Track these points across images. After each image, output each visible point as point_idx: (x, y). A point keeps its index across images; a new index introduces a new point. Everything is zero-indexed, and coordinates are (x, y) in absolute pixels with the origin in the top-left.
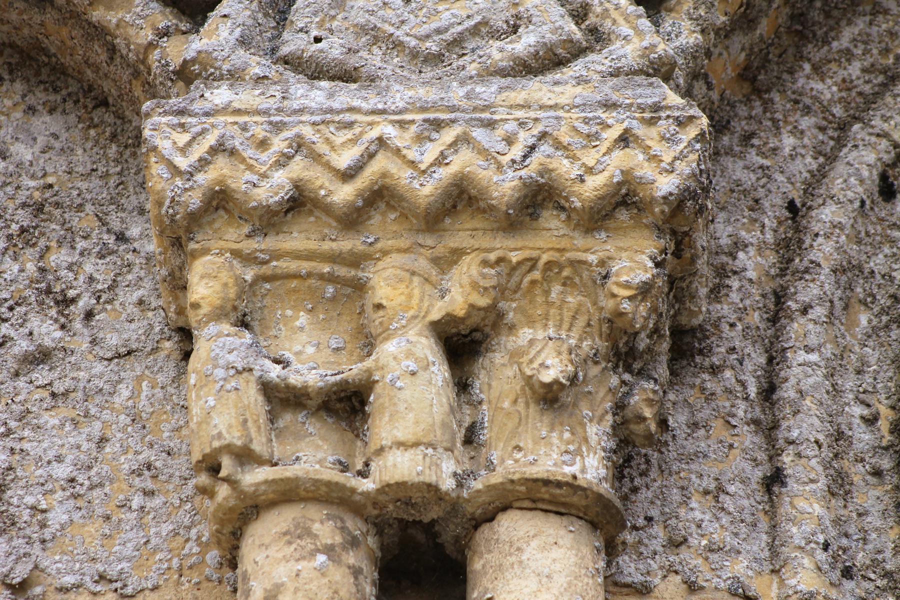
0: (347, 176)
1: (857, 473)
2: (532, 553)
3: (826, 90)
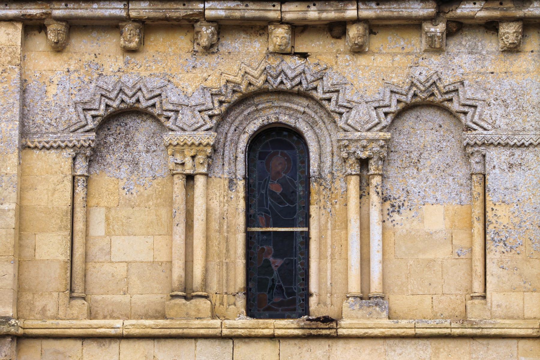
0: (182, 142)
1: (231, 162)
2: (200, 179)
3: (229, 120)
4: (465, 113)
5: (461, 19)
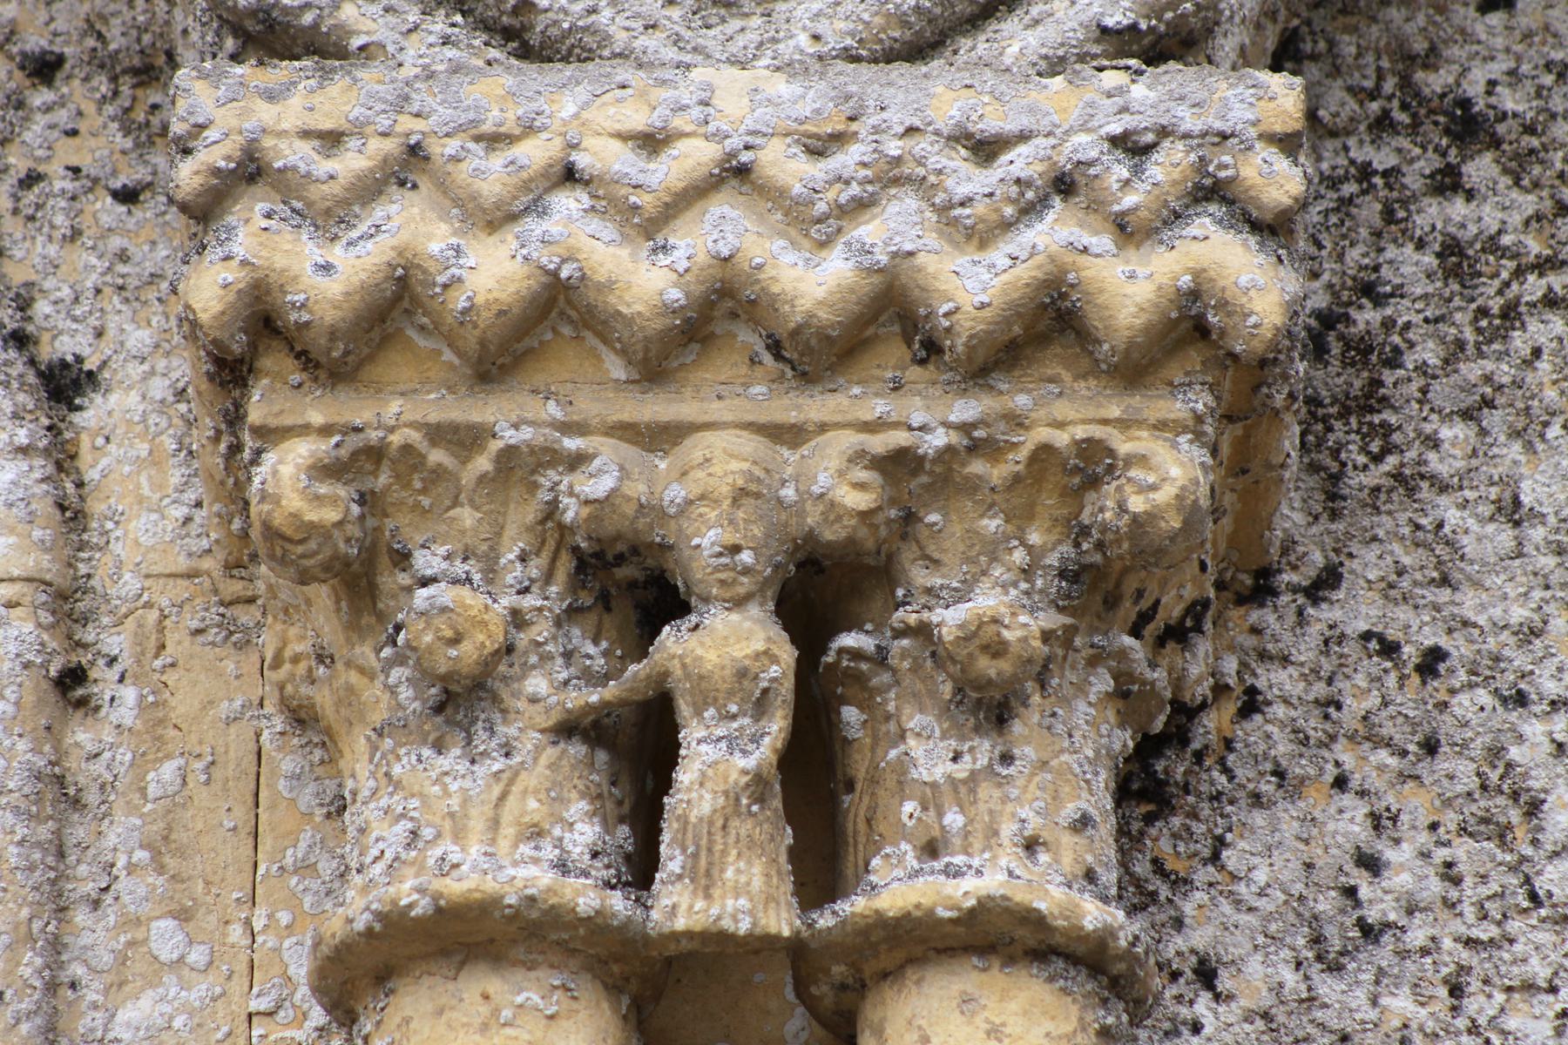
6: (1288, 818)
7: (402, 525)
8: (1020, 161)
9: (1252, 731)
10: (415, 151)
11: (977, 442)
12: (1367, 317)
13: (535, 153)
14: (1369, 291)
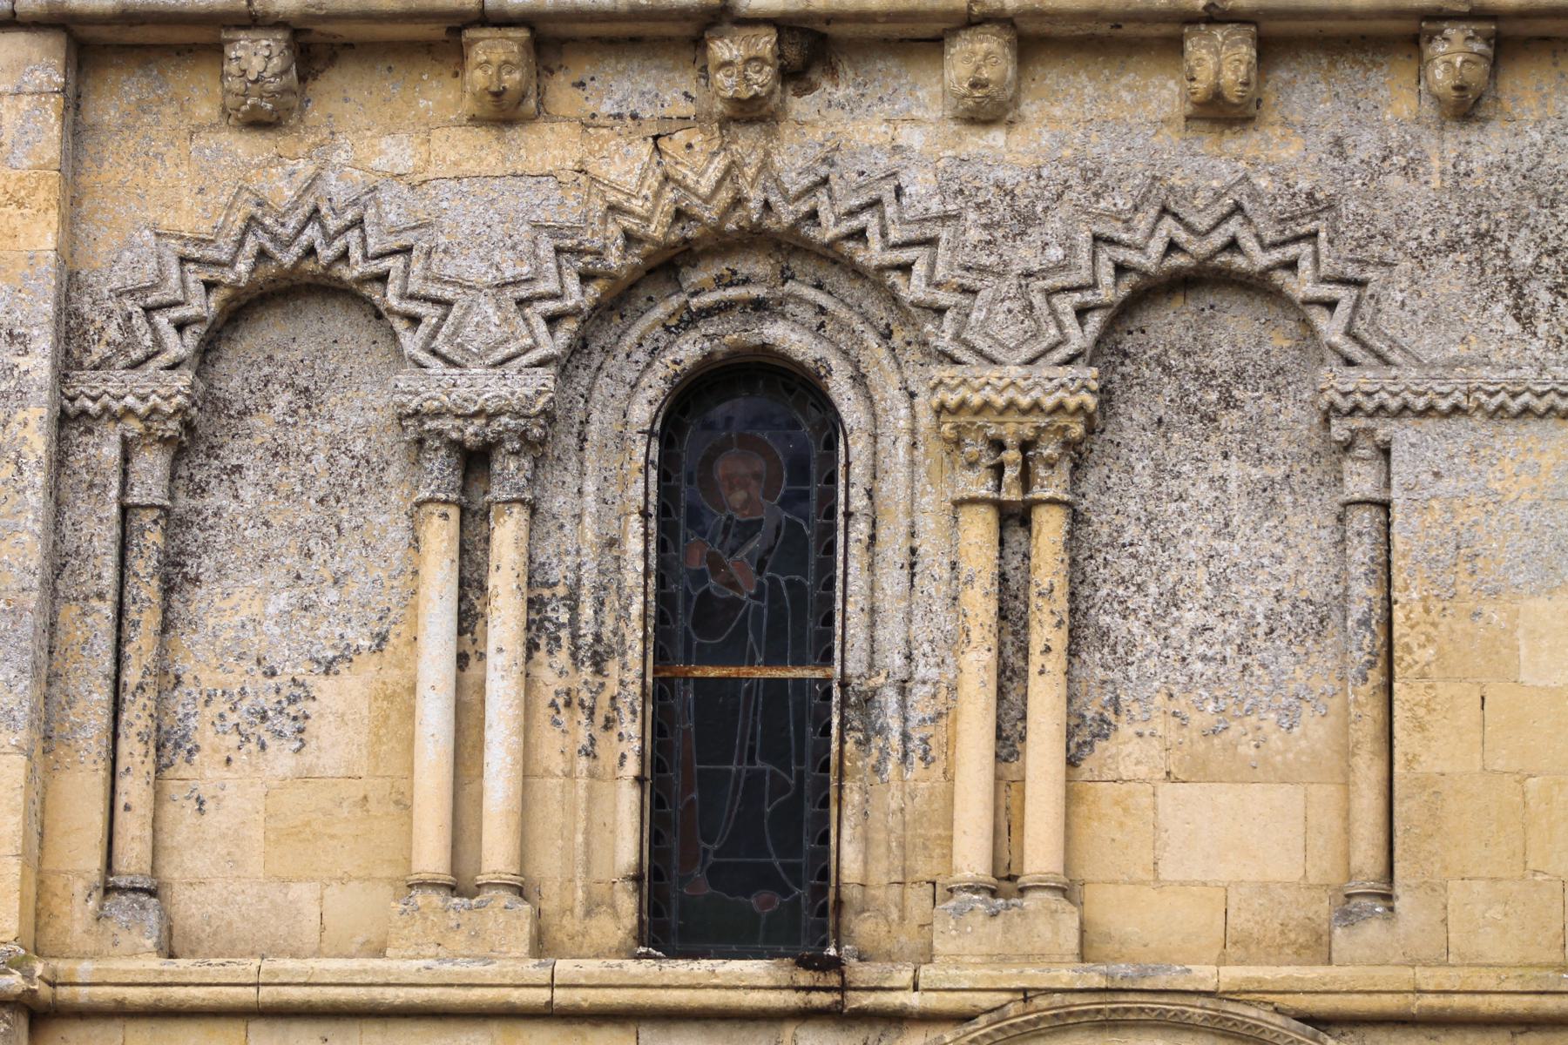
4: (1331, 305)
5: (828, 22)
6: (1097, 469)
7: (963, 435)
8: (1055, 382)
9: (1091, 456)
10: (965, 380)
11: (1049, 425)
12: (1110, 386)
13: (983, 380)
14: (1110, 382)
